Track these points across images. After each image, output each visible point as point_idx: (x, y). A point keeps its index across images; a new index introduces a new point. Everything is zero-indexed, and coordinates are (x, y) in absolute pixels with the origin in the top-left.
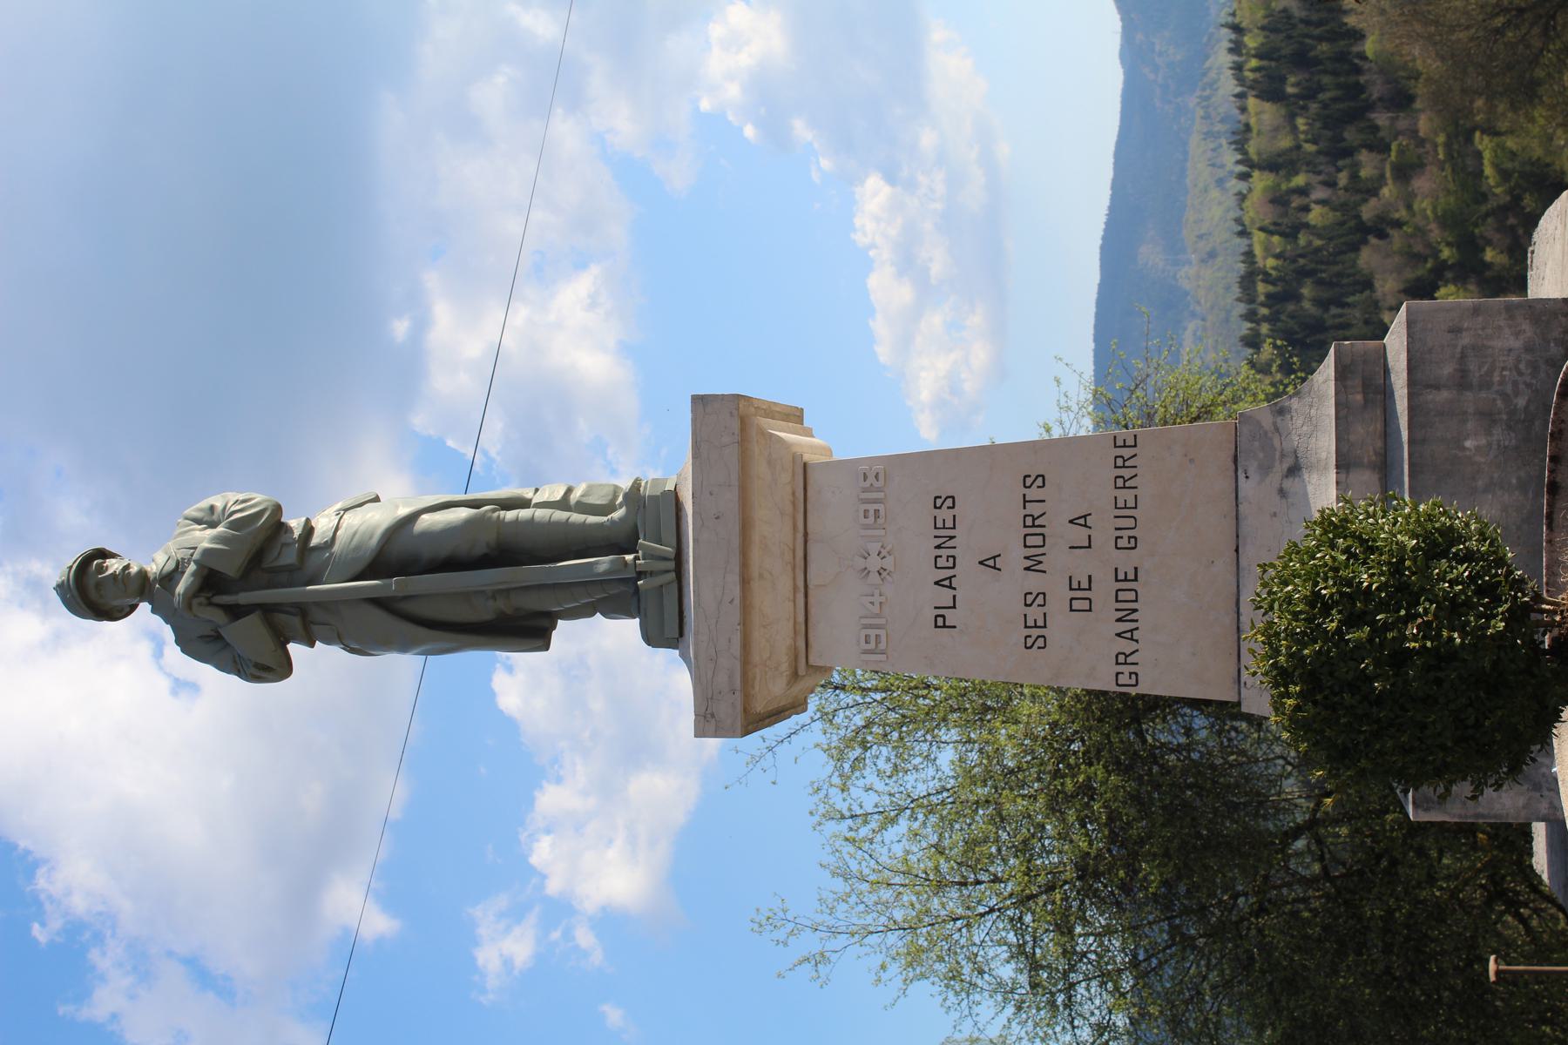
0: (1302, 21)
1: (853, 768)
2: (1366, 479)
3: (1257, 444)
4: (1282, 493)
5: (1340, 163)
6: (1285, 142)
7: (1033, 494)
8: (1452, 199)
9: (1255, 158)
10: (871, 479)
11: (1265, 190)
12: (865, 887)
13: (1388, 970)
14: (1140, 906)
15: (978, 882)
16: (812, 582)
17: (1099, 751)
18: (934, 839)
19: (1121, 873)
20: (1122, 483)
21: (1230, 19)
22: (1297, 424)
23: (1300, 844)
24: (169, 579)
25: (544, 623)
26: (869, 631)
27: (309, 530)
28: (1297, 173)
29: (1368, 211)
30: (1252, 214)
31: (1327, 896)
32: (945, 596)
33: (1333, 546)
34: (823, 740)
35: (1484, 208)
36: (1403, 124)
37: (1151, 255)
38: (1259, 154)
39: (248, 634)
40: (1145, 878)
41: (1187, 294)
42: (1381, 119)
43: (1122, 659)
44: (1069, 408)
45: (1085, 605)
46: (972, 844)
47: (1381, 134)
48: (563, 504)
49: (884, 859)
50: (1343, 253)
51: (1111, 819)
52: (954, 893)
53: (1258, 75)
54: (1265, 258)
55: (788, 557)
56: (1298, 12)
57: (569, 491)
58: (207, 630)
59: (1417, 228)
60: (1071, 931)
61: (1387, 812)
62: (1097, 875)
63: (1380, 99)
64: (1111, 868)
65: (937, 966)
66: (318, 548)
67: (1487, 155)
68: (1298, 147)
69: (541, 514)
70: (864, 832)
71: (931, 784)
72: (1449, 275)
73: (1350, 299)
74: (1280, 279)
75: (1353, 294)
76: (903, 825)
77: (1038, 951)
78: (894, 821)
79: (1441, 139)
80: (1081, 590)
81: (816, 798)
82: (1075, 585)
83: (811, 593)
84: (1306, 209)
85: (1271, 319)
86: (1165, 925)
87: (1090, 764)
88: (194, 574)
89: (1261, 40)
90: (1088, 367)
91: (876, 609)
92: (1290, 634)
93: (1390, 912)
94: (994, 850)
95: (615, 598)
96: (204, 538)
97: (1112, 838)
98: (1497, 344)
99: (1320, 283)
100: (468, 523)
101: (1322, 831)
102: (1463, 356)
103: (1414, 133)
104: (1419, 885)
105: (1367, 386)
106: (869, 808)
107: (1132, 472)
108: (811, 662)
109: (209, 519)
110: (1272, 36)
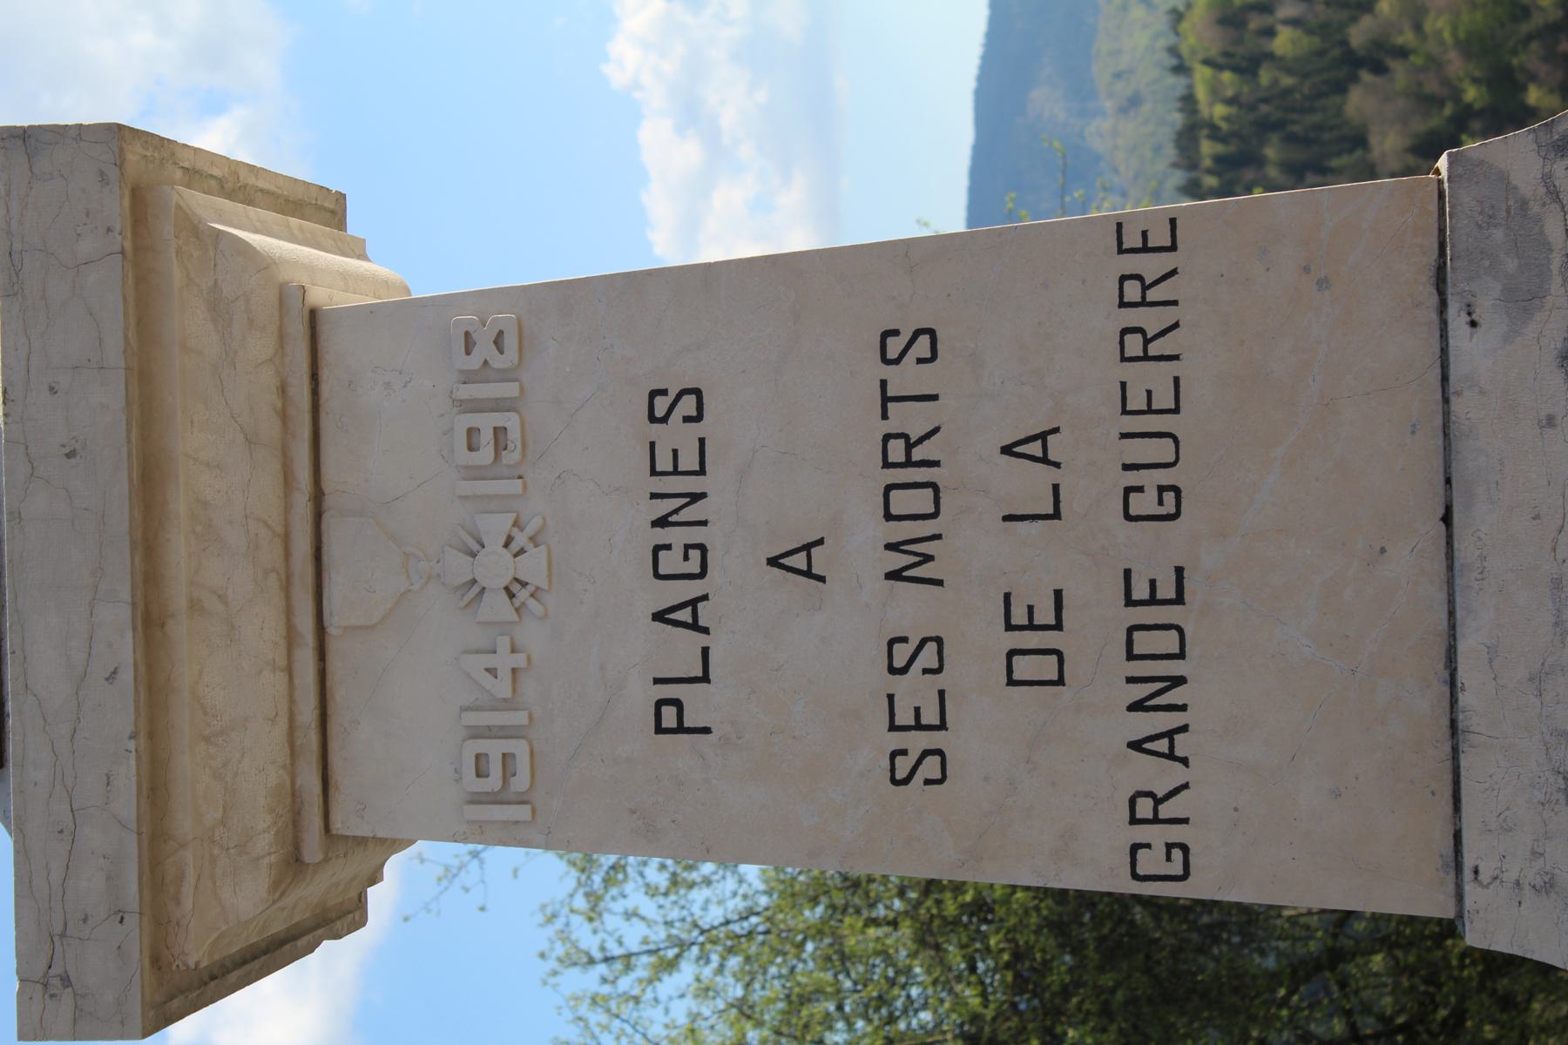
1: (608, 881)
3: (1498, 234)
7: (905, 378)
8: (1479, 15)
10: (484, 349)
16: (335, 622)
20: (1139, 346)
26: (483, 746)
29: (1359, 34)
30: (1192, 40)
32: (681, 650)
35: (1525, 28)
43: (1147, 808)
46: (798, 1000)
51: (1018, 956)
54: (1211, 104)
55: (271, 554)
71: (731, 904)
72: (1476, 125)
73: (1335, 163)
74: (1235, 135)
75: (1339, 154)
76: (687, 971)
78: (671, 965)
80: (1034, 636)
81: (550, 931)
82: (1019, 617)
83: (333, 647)
84: (1270, 33)
91: (503, 688)
94: (832, 1007)
99: (1291, 139)
101: (1352, 969)
106: (633, 944)
107: (1165, 316)
108: (338, 826)
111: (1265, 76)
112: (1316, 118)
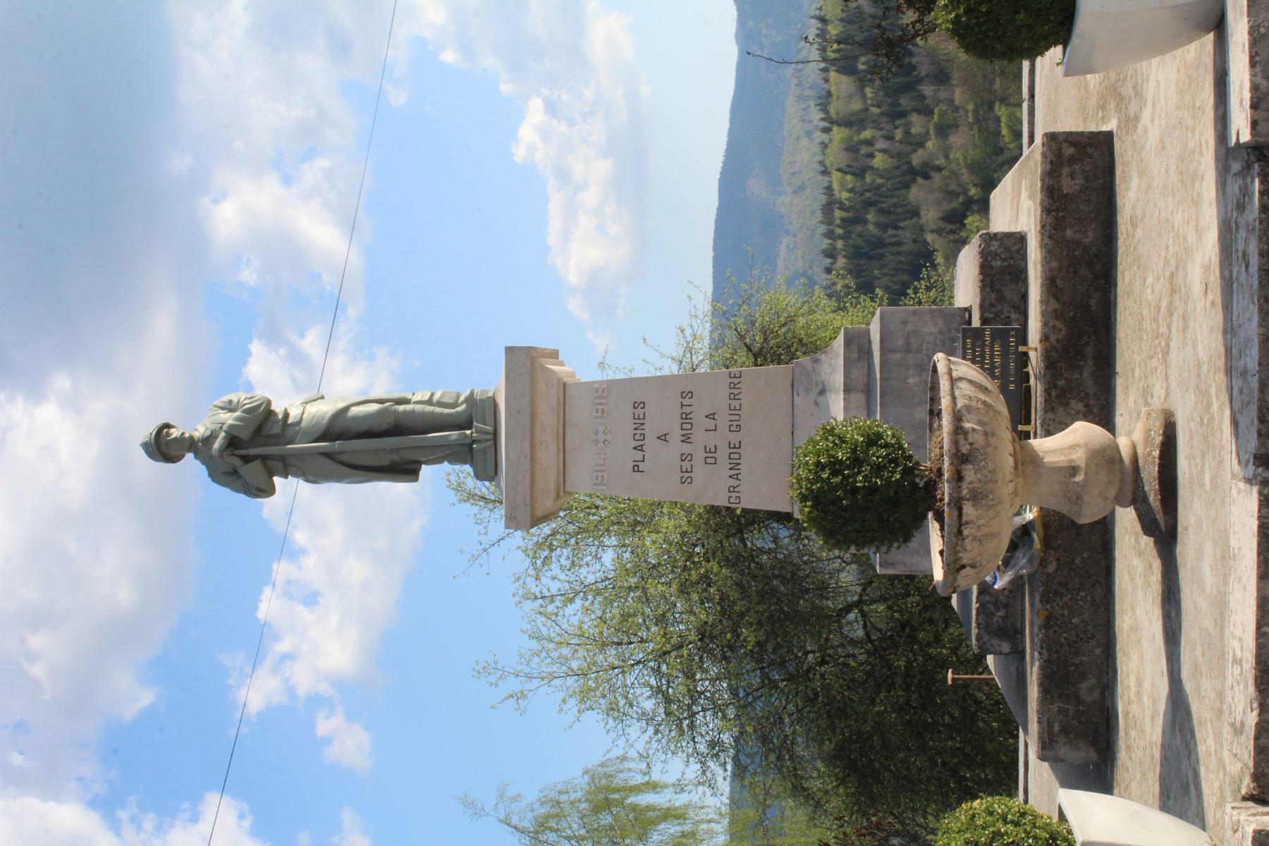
0: (871, 16)
1: (543, 563)
2: (858, 398)
4: (816, 404)
5: (897, 122)
6: (857, 106)
7: (686, 401)
8: (978, 151)
9: (834, 116)
11: (842, 140)
12: (552, 646)
13: (908, 702)
14: (740, 660)
15: (631, 643)
17: (714, 554)
18: (599, 613)
19: (729, 635)
20: (733, 397)
21: (818, 12)
22: (824, 368)
23: (851, 616)
24: (208, 440)
25: (415, 466)
27: (286, 415)
28: (865, 129)
29: (917, 159)
31: (867, 652)
32: (639, 455)
33: (827, 439)
34: (522, 544)
35: (1001, 159)
36: (943, 94)
37: (756, 187)
38: (837, 114)
39: (253, 471)
40: (745, 640)
41: (782, 217)
42: (927, 90)
43: (732, 489)
44: (696, 316)
45: (713, 461)
46: (625, 617)
47: (927, 101)
48: (429, 402)
49: (565, 626)
50: (897, 189)
51: (721, 599)
52: (612, 651)
53: (837, 55)
56: (868, 9)
57: (432, 395)
58: (228, 469)
59: (952, 172)
60: (693, 676)
61: (908, 595)
62: (712, 638)
63: (927, 76)
64: (722, 632)
65: (602, 701)
66: (292, 425)
67: (1004, 119)
68: (866, 110)
69: (418, 407)
70: (551, 608)
72: (975, 208)
73: (902, 224)
76: (578, 602)
77: (670, 691)
78: (572, 600)
79: (970, 107)
80: (711, 454)
84: (872, 156)
85: (845, 237)
86: (758, 672)
87: (708, 561)
88: (225, 438)
89: (840, 28)
90: (709, 287)
92: (807, 479)
93: (910, 663)
95: (461, 453)
96: (229, 418)
97: (723, 612)
98: (925, 330)
99: (882, 211)
100: (379, 412)
101: (865, 608)
102: (908, 337)
103: (951, 101)
104: (929, 645)
105: (860, 349)
109: (230, 407)
110: (849, 27)
111: (869, 178)
112: (895, 200)
